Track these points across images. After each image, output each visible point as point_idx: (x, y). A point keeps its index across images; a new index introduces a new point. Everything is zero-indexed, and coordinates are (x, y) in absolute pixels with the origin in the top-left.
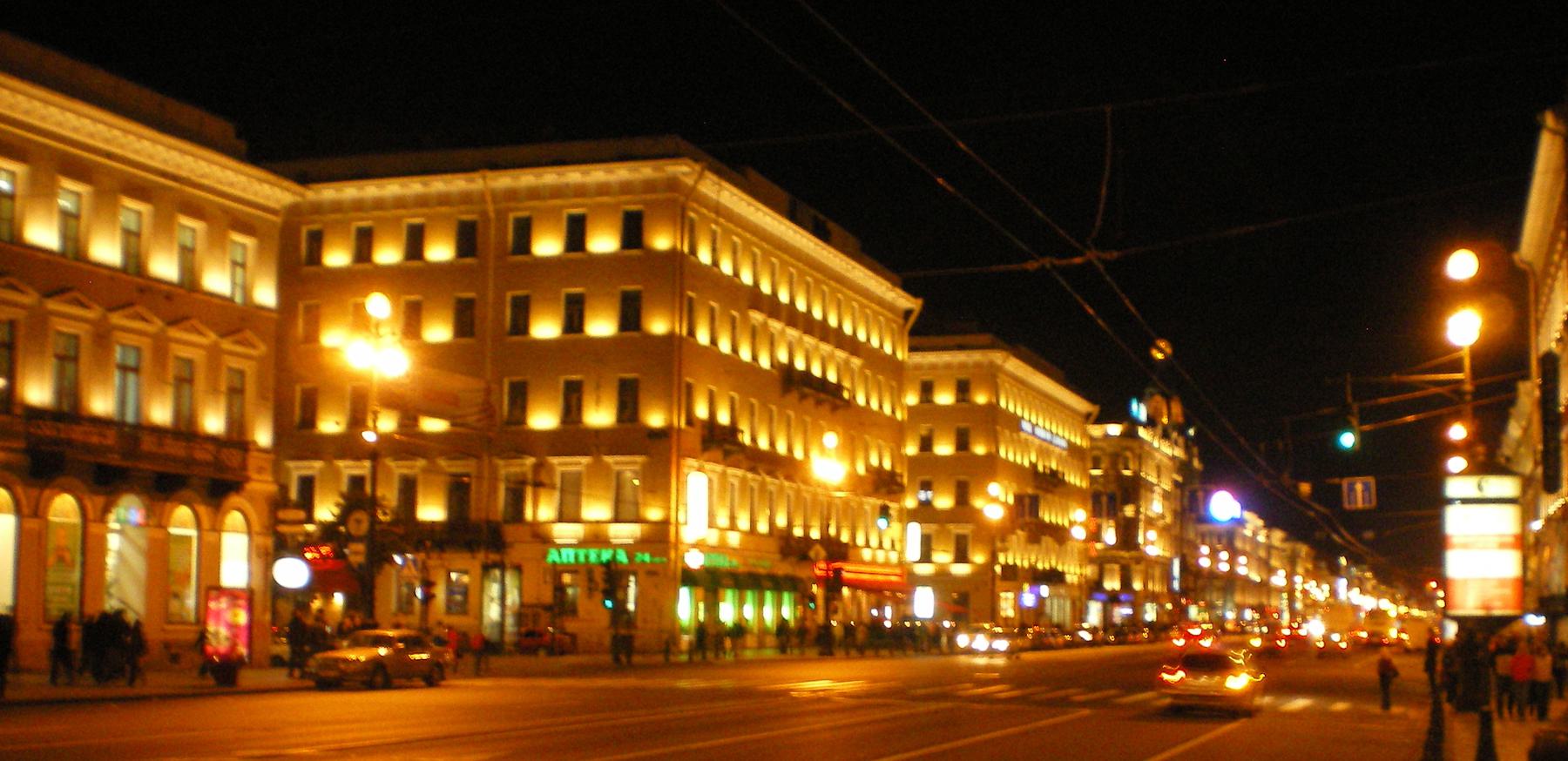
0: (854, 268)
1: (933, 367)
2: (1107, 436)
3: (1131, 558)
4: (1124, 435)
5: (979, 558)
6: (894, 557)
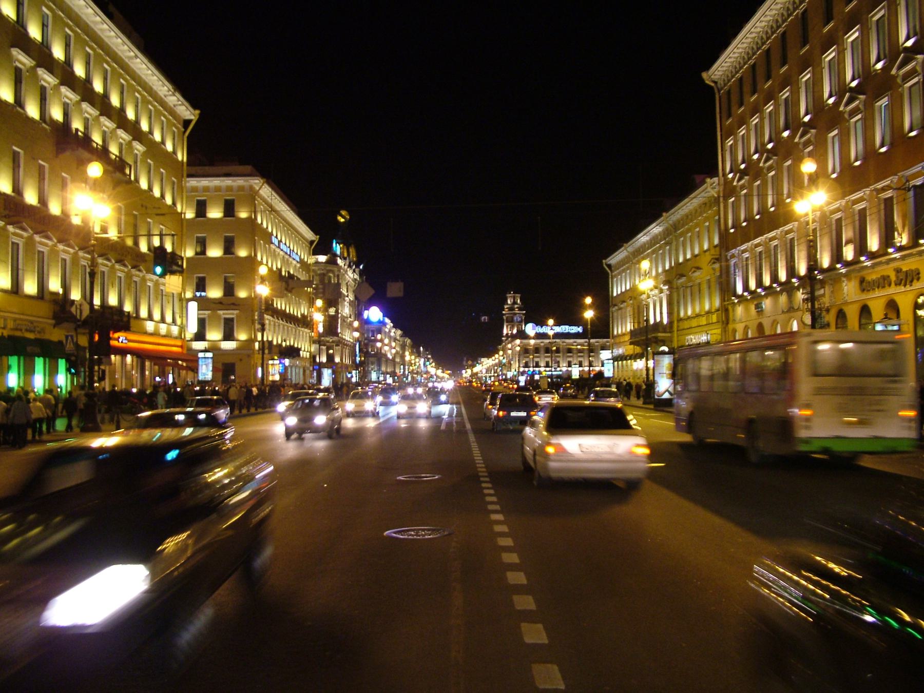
0: (136, 57)
1: (206, 189)
2: (317, 263)
3: (333, 342)
4: (327, 262)
5: (242, 336)
6: (175, 330)
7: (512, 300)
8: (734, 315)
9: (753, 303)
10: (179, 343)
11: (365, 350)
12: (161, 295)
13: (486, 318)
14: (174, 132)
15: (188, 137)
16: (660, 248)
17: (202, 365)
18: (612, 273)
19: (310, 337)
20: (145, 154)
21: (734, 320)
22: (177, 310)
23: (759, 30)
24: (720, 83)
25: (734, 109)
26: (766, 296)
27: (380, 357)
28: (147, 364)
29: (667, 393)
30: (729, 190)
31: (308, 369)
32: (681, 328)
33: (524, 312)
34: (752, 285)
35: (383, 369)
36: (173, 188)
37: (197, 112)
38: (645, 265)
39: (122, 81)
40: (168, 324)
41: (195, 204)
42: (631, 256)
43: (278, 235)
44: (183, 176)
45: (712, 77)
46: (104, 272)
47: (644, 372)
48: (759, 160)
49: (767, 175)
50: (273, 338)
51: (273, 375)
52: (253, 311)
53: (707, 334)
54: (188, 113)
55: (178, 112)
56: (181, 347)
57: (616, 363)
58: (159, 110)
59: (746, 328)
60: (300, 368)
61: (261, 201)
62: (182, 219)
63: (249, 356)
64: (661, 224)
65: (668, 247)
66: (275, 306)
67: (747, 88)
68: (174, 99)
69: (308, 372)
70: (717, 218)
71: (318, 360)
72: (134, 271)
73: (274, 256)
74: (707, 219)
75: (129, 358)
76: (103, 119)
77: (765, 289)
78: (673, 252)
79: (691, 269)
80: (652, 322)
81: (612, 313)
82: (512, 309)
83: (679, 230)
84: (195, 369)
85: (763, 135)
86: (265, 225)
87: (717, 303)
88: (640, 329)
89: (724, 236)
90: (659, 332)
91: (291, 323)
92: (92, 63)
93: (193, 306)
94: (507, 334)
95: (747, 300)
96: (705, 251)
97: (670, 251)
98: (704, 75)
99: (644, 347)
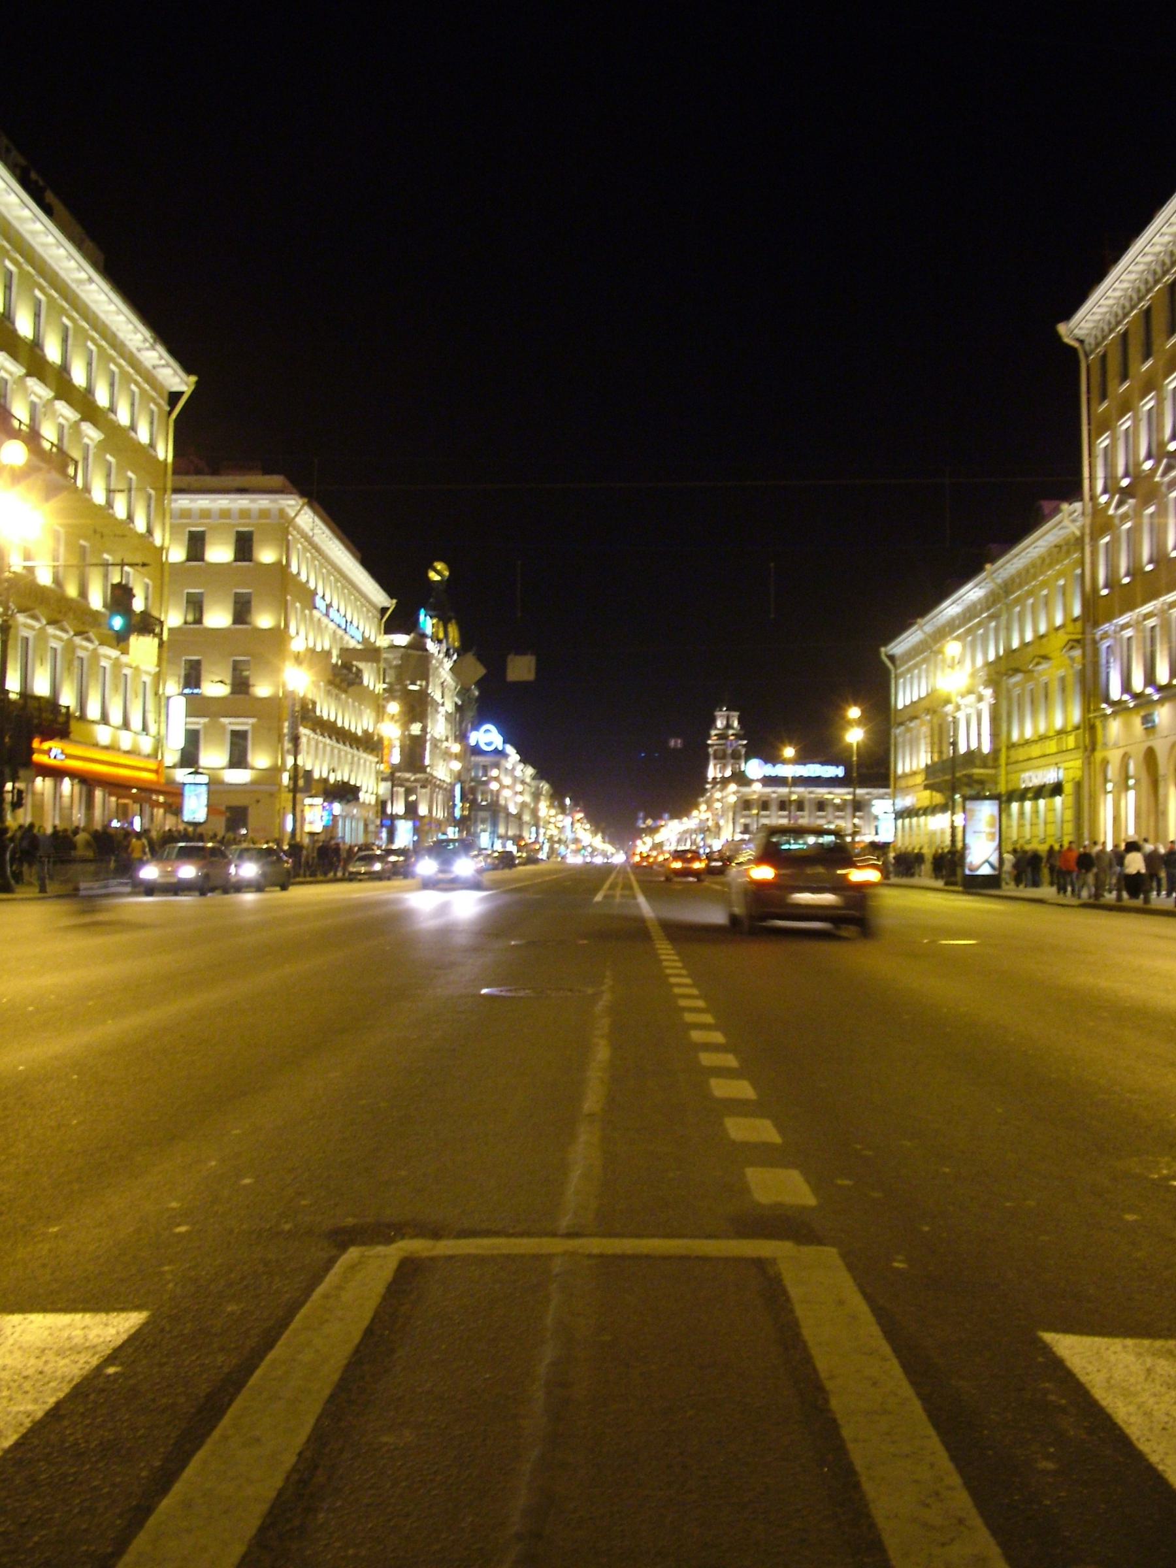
0: (91, 280)
1: (205, 514)
3: (416, 781)
5: (260, 759)
7: (726, 721)
8: (1104, 736)
9: (1138, 713)
10: (152, 765)
11: (471, 797)
12: (121, 680)
13: (679, 741)
14: (152, 412)
15: (176, 421)
16: (979, 625)
17: (190, 796)
18: (896, 669)
19: (378, 772)
20: (103, 446)
21: (1105, 744)
22: (151, 706)
23: (1157, 249)
24: (1090, 341)
25: (1112, 382)
26: (1161, 701)
27: (495, 811)
28: (98, 794)
29: (987, 865)
30: (1101, 524)
31: (373, 822)
32: (1012, 759)
33: (745, 742)
34: (1138, 684)
35: (501, 830)
36: (149, 506)
37: (193, 379)
38: (952, 648)
39: (65, 320)
40: (135, 733)
41: (187, 536)
42: (929, 640)
43: (326, 592)
44: (165, 491)
45: (1076, 331)
46: (27, 639)
47: (948, 831)
48: (1153, 470)
49: (1166, 496)
50: (313, 765)
51: (311, 823)
52: (280, 720)
53: (1059, 768)
54: (177, 380)
55: (160, 377)
56: (156, 772)
57: (900, 822)
58: (128, 373)
59: (1126, 757)
60: (358, 820)
61: (299, 536)
62: (162, 564)
63: (272, 795)
64: (983, 584)
65: (993, 624)
66: (318, 713)
67: (1135, 351)
68: (155, 357)
69: (372, 828)
70: (1078, 571)
71: (389, 811)
72: (78, 640)
73: (319, 628)
74: (1060, 575)
75: (67, 782)
76: (32, 382)
77: (1160, 689)
78: (1002, 634)
79: (1034, 658)
80: (962, 749)
81: (896, 738)
82: (722, 736)
83: (1013, 593)
84: (175, 809)
85: (1160, 429)
86: (303, 578)
87: (1076, 715)
88: (943, 762)
89: (1091, 602)
90: (976, 767)
91: (344, 744)
92: (14, 289)
93: (178, 706)
94: (714, 779)
95: (1128, 709)
96: (1057, 629)
97: (997, 629)
98: (1062, 328)
99: (948, 793)
